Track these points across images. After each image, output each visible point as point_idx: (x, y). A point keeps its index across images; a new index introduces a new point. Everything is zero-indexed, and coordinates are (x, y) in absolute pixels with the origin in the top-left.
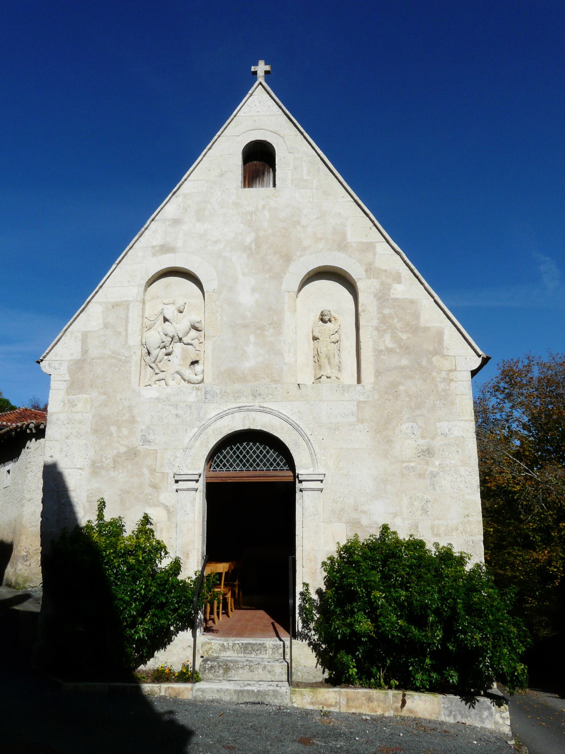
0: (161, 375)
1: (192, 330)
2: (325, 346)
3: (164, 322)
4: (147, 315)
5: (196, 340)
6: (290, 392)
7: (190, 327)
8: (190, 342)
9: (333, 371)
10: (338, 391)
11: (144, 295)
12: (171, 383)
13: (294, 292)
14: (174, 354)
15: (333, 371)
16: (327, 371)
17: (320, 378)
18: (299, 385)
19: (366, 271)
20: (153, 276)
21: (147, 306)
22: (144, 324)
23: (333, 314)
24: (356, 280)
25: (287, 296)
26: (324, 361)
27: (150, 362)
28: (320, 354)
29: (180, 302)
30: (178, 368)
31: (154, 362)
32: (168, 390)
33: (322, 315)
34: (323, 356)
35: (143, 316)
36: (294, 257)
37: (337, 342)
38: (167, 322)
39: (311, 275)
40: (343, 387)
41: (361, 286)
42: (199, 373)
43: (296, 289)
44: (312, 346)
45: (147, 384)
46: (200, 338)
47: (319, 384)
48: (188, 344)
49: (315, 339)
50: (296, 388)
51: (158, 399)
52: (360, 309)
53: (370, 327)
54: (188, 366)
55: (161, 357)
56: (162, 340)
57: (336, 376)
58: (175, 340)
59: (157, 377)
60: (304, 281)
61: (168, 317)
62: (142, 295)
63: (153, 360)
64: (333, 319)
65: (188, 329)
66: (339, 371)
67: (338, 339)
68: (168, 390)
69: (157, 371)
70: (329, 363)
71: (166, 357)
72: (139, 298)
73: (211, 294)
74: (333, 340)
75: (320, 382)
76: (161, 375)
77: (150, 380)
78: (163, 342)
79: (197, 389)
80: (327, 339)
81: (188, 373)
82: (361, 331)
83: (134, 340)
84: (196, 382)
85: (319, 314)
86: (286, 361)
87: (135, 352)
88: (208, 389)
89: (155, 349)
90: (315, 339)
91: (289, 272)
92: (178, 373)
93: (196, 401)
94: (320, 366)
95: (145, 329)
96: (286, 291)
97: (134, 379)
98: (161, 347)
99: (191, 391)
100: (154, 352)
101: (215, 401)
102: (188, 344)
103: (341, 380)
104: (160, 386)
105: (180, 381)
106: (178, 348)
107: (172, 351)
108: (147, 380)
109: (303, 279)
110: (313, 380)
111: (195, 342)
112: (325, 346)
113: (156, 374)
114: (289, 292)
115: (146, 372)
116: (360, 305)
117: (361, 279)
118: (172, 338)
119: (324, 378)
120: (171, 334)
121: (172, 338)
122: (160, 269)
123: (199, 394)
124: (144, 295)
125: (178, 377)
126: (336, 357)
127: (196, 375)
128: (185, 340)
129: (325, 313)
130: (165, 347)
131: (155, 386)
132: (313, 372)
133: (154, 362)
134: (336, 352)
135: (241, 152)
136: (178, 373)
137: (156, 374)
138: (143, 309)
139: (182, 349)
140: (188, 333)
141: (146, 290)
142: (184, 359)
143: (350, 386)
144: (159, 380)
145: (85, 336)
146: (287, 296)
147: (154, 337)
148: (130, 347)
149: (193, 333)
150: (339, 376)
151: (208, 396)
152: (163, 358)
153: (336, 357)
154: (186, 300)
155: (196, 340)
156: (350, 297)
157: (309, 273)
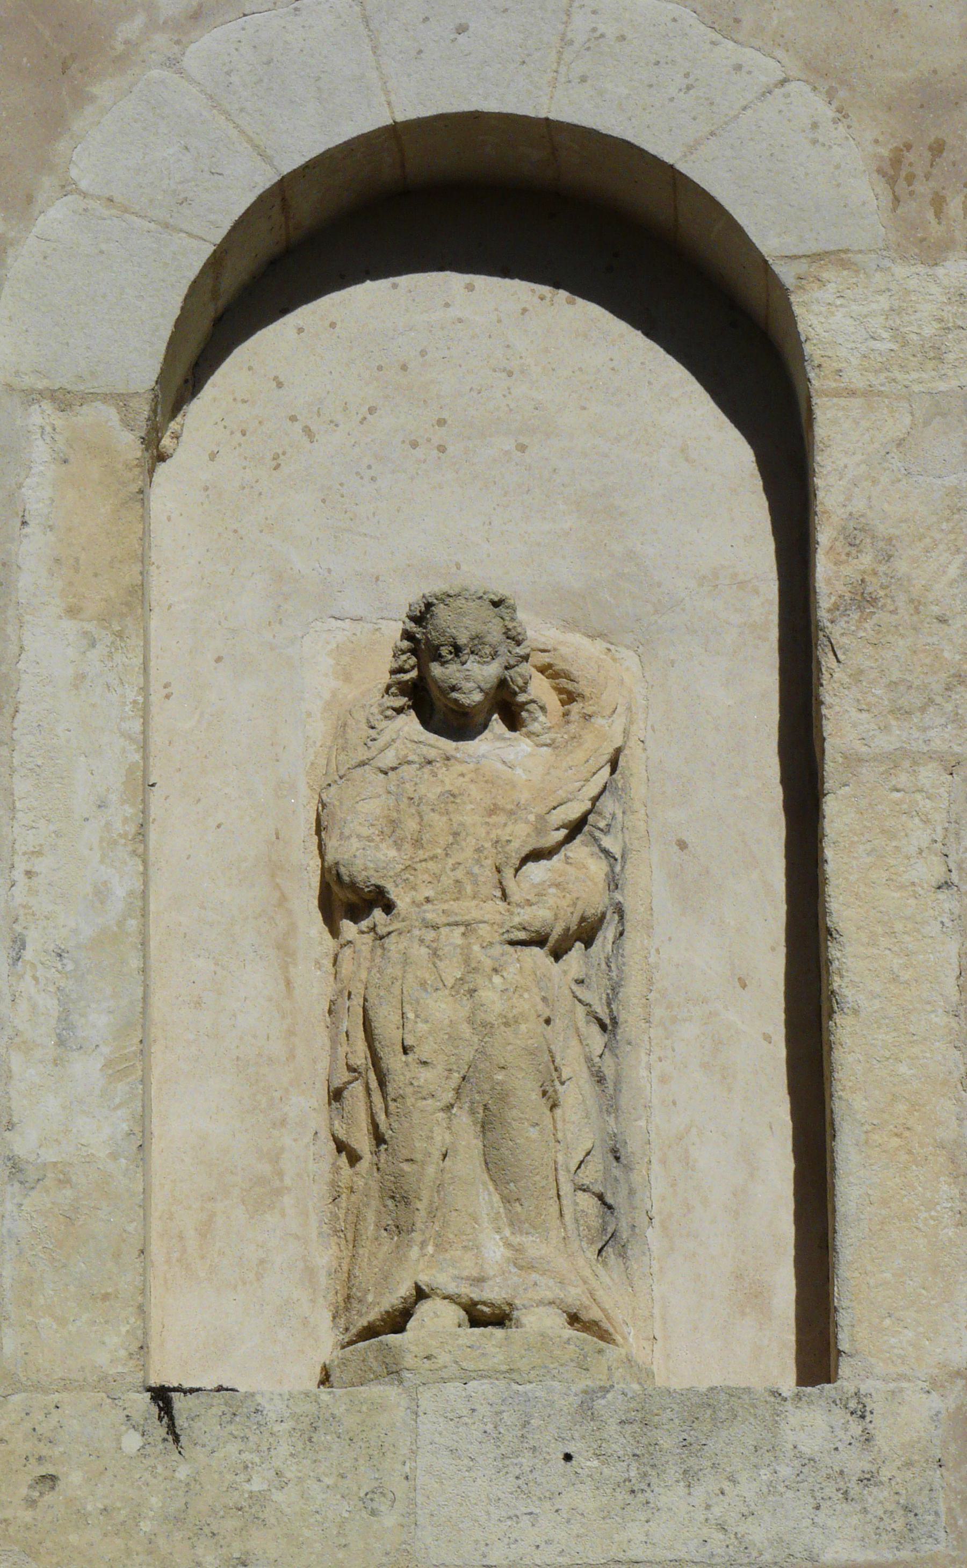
2: (454, 986)
6: (73, 1479)
9: (535, 1247)
10: (586, 1463)
13: (121, 400)
15: (535, 1247)
16: (481, 1248)
17: (398, 1320)
18: (162, 1397)
19: (894, 171)
23: (539, 631)
24: (786, 273)
25: (40, 451)
26: (439, 1136)
28: (394, 1061)
33: (424, 641)
34: (424, 1081)
36: (130, 29)
37: (586, 933)
39: (306, 210)
40: (641, 1418)
41: (833, 327)
43: (141, 360)
44: (315, 986)
47: (389, 1392)
49: (348, 900)
50: (130, 1436)
52: (829, 575)
53: (929, 774)
57: (575, 1295)
60: (231, 281)
64: (540, 689)
66: (610, 1242)
67: (594, 898)
70: (496, 1166)
74: (538, 916)
75: (393, 1371)
80: (468, 909)
82: (838, 813)
85: (392, 631)
86: (23, 1144)
90: (348, 900)
91: (67, 188)
94: (398, 1196)
96: (31, 397)
103: (632, 1340)
109: (216, 263)
110: (325, 1344)
112: (454, 986)
114: (64, 400)
116: (825, 535)
117: (837, 258)
119: (437, 1321)
126: (577, 1093)
129: (454, 624)
132: (325, 1256)
134: (575, 1048)
135: (661, 137)
143: (710, 1409)
145: (828, 581)
146: (40, 451)
150: (607, 1293)
153: (577, 1093)
156: (729, 455)
157: (281, 194)
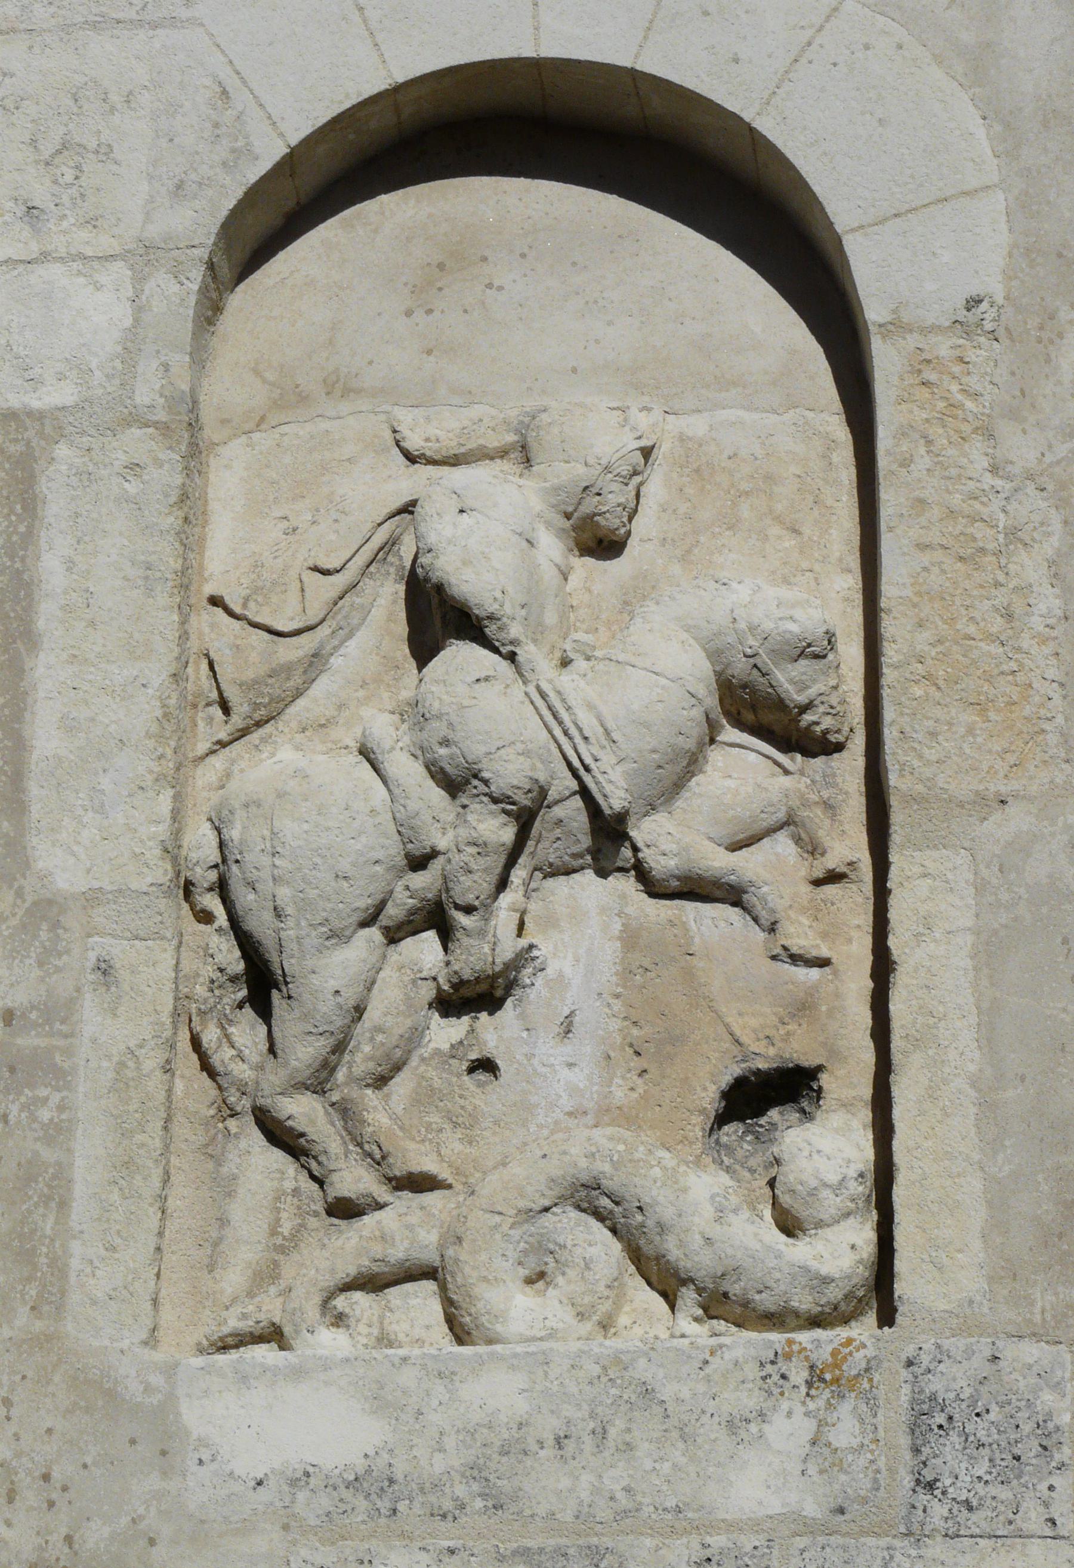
0: (403, 1228)
1: (731, 734)
3: (423, 650)
4: (221, 567)
5: (782, 845)
7: (712, 702)
8: (717, 861)
11: (199, 358)
12: (515, 1308)
14: (536, 992)
20: (290, 164)
21: (229, 477)
22: (194, 645)
27: (274, 1077)
29: (596, 435)
30: (592, 1149)
31: (318, 1081)
32: (494, 1390)
35: (185, 581)
38: (461, 656)
42: (830, 1203)
45: (233, 1323)
46: (816, 817)
48: (695, 889)
51: (376, 1489)
54: (697, 1125)
55: (399, 1026)
56: (404, 830)
58: (546, 845)
59: (352, 1246)
61: (472, 581)
62: (180, 360)
63: (303, 1052)
65: (697, 730)
68: (494, 1390)
69: (353, 1179)
71: (446, 1032)
72: (147, 392)
73: (944, 347)
76: (403, 1228)
77: (266, 1275)
78: (418, 862)
79: (816, 1378)
81: (706, 1205)
83: (99, 834)
84: (804, 1302)
87: (105, 969)
88: (952, 1381)
89: (337, 936)
92: (593, 1199)
93: (812, 1509)
95: (211, 726)
97: (104, 1264)
98: (394, 912)
99: (750, 1400)
100: (327, 971)
101: (1033, 1518)
102: (695, 889)
104: (385, 1340)
105: (615, 1284)
106: (576, 932)
107: (524, 957)
108: (233, 1279)
111: (773, 869)
113: (345, 1210)
115: (226, 1188)
118: (525, 820)
120: (510, 772)
121: (525, 820)
122: (374, 83)
123: (845, 1431)
124: (199, 358)
125: (600, 1247)
127: (789, 1225)
128: (667, 839)
130: (436, 918)
131: (330, 1341)
133: (318, 1081)
136: (593, 1199)
137: (345, 1210)
138: (190, 508)
139: (630, 939)
140: (691, 764)
141: (210, 309)
142: (647, 1048)
144: (372, 1283)
147: (323, 804)
148: (46, 911)
149: (743, 773)
151: (949, 1457)
152: (415, 1036)
154: (667, 431)
155: (782, 845)
